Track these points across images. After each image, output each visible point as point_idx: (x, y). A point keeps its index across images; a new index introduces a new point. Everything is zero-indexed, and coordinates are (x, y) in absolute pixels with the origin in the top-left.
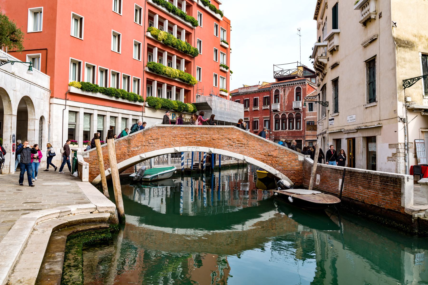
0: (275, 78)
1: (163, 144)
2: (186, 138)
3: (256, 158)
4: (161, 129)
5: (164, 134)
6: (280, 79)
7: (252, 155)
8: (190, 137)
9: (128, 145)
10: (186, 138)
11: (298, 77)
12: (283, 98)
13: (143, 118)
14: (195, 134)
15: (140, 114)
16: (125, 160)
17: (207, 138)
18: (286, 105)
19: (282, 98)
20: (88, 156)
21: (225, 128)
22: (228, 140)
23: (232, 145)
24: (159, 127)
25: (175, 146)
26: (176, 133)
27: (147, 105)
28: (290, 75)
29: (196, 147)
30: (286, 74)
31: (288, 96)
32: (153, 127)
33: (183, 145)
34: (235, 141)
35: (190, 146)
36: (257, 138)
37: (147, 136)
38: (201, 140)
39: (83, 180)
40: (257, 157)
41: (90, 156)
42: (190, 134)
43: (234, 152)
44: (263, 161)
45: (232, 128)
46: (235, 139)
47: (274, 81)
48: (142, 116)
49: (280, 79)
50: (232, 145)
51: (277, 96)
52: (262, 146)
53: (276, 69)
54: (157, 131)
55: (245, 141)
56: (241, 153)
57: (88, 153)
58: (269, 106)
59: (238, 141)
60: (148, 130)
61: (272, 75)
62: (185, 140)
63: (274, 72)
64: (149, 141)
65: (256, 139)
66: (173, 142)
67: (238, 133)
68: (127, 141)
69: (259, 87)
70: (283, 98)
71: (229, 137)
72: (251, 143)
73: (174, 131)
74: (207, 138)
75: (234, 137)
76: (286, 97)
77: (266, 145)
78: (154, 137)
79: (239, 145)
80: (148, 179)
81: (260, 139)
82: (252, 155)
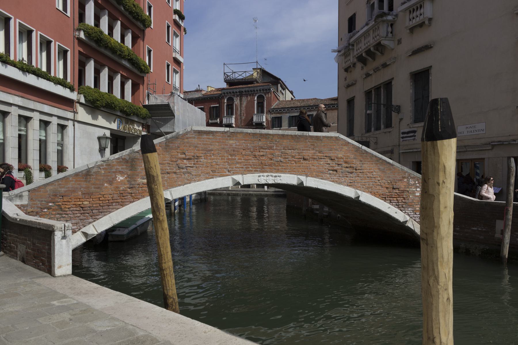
0: (226, 81)
1: (209, 170)
2: (255, 156)
3: (375, 194)
4: (205, 136)
5: (211, 147)
6: (231, 83)
7: (368, 188)
8: (262, 153)
9: (129, 172)
10: (255, 156)
11: (257, 82)
12: (239, 109)
13: (76, 123)
14: (271, 148)
15: (70, 115)
16: (123, 206)
17: (293, 157)
18: (243, 118)
19: (237, 109)
20: (25, 201)
21: (324, 137)
22: (329, 162)
23: (336, 171)
24: (200, 133)
25: (234, 174)
26: (234, 146)
27: (83, 100)
28: (245, 79)
29: (274, 174)
30: (241, 77)
31: (246, 107)
32: (187, 133)
33: (250, 172)
34: (341, 162)
35: (263, 172)
36: (376, 156)
37: (174, 152)
38: (282, 159)
39: (58, 272)
40: (376, 191)
41: (31, 199)
42: (262, 148)
43: (340, 183)
44: (385, 199)
45: (336, 138)
46: (341, 158)
47: (224, 85)
48: (74, 121)
49: (231, 83)
50: (336, 171)
51: (230, 107)
52: (383, 171)
53: (227, 70)
54: (195, 141)
55: (357, 163)
56: (350, 185)
57: (26, 194)
58: (218, 120)
59: (346, 162)
60: (177, 137)
61: (222, 78)
62: (253, 161)
63: (225, 73)
64: (179, 162)
65: (374, 158)
66: (229, 164)
67: (346, 148)
68: (127, 162)
69: (203, 93)
70: (239, 109)
71: (332, 154)
72: (367, 166)
73: (231, 142)
74: (293, 157)
75: (340, 156)
76: (243, 108)
77: (390, 170)
78: (189, 154)
79: (347, 170)
80: (122, 236)
81: (380, 159)
82: (368, 188)
